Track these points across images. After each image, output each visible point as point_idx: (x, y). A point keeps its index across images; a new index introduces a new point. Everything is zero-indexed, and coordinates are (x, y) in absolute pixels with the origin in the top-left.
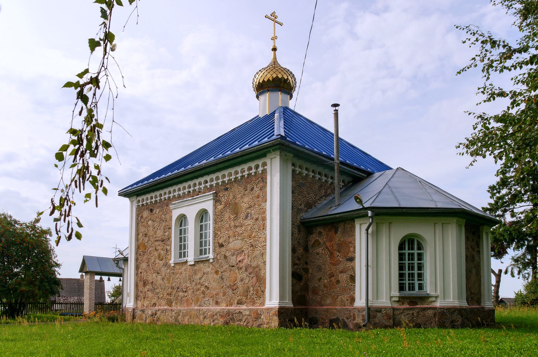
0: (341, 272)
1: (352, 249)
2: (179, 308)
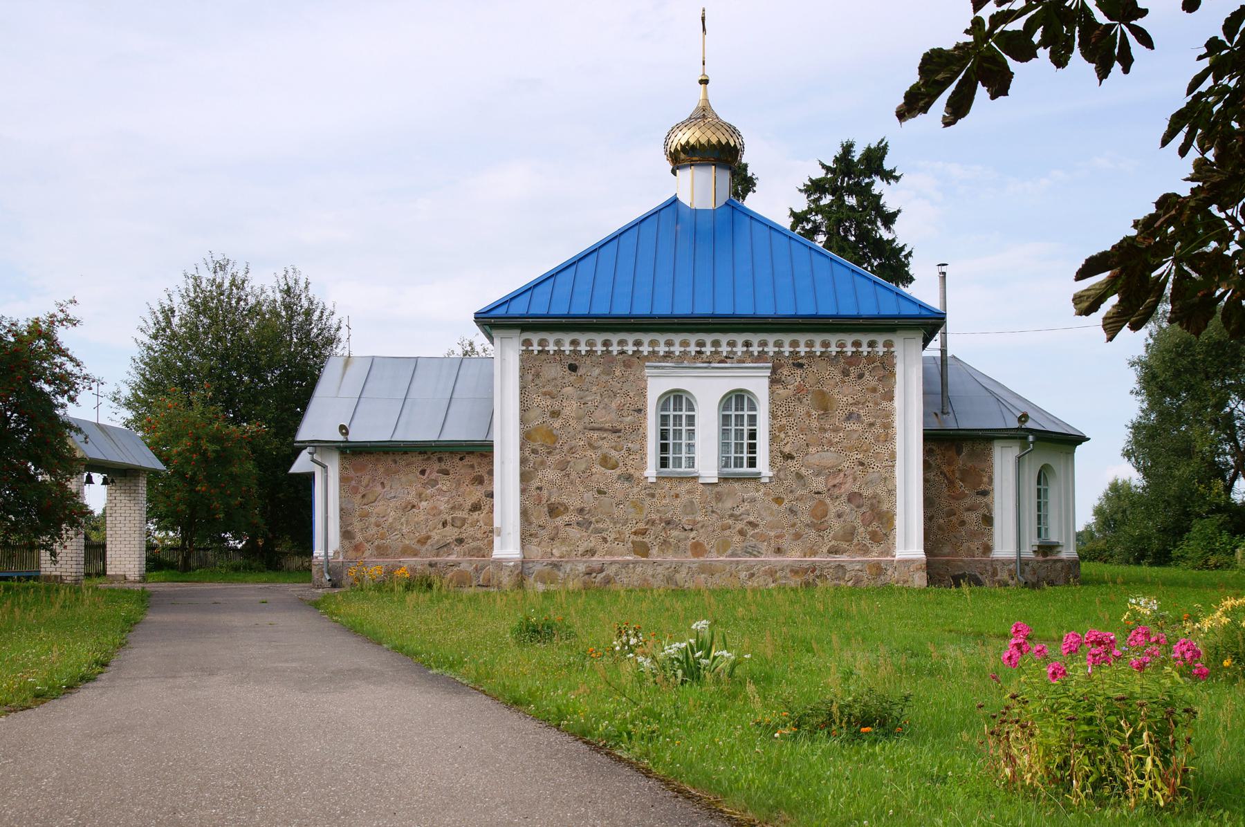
0: (968, 510)
1: (985, 479)
2: (670, 558)
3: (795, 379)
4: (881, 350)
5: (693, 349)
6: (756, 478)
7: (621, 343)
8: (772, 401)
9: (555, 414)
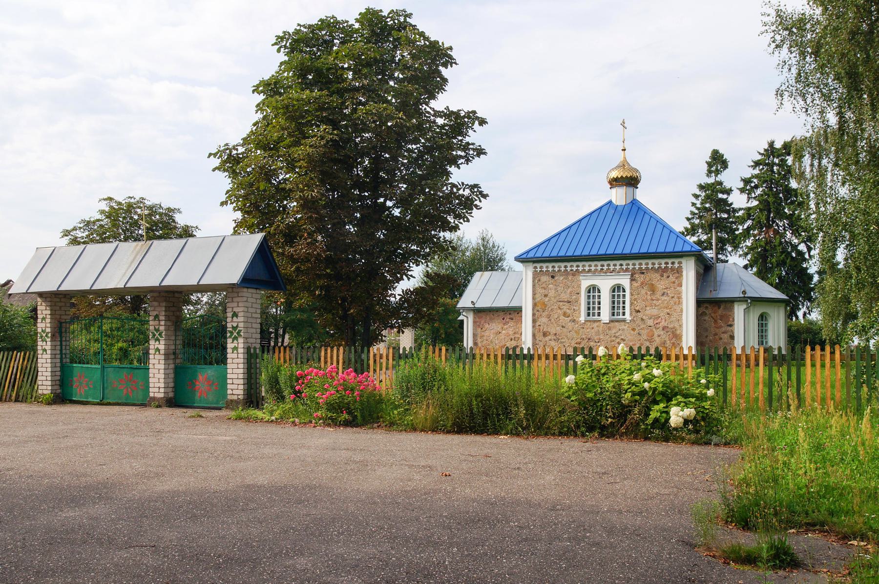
3: (640, 278)
4: (676, 265)
5: (599, 268)
6: (624, 321)
7: (571, 266)
8: (631, 289)
9: (546, 296)
